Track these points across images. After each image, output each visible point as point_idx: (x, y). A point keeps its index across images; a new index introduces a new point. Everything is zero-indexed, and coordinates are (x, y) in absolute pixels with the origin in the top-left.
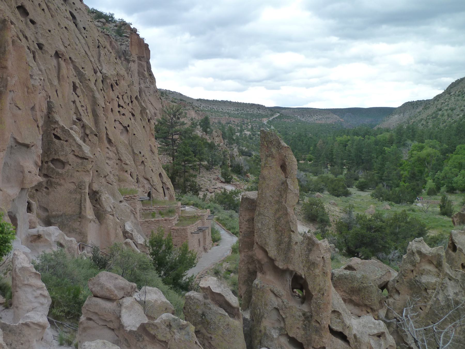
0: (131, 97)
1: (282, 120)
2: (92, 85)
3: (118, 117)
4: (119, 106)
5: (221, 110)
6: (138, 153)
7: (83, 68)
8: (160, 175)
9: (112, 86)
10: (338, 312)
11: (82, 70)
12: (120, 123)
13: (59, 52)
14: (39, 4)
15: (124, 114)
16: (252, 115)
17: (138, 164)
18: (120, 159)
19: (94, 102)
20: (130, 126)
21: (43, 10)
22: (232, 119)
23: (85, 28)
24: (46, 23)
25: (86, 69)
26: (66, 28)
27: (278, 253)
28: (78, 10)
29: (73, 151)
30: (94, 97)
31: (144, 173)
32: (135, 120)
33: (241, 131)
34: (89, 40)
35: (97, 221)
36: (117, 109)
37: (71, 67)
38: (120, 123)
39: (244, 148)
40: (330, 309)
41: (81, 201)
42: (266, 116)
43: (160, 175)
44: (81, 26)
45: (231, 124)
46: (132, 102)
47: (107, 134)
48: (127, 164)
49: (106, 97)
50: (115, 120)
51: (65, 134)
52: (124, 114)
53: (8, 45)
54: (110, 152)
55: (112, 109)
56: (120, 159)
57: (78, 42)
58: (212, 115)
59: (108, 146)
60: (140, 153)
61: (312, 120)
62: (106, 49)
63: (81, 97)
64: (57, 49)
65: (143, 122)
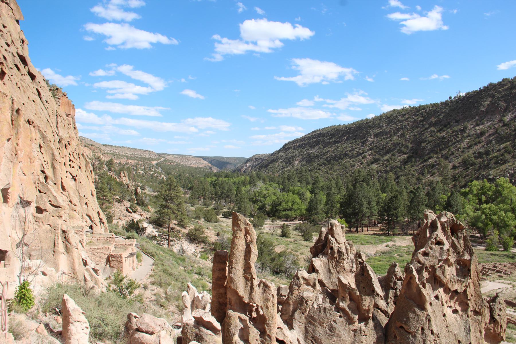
0: (79, 154)
1: (167, 163)
2: (52, 145)
3: (69, 169)
4: (70, 160)
5: (122, 154)
6: (83, 196)
7: (45, 132)
8: (98, 213)
9: (66, 146)
10: (281, 328)
11: (45, 133)
12: (71, 174)
13: (30, 121)
14: (17, 83)
15: (73, 167)
16: (145, 159)
17: (82, 204)
18: (71, 202)
19: (54, 159)
20: (78, 176)
21: (19, 88)
22: (130, 161)
23: (47, 102)
24: (21, 98)
25: (47, 133)
26: (34, 101)
27: (245, 293)
28: (42, 88)
29: (50, 201)
30: (53, 155)
31: (87, 211)
32: (81, 171)
33: (136, 170)
34: (50, 110)
35: (66, 253)
36: (68, 163)
37: (37, 131)
38: (71, 174)
39: (139, 183)
40: (277, 327)
41: (55, 238)
42: (155, 160)
43: (98, 213)
44: (44, 99)
45: (129, 164)
46: (79, 158)
47: (62, 183)
48: (75, 205)
49: (61, 154)
50: (67, 172)
51: (44, 188)
52: (73, 167)
53: (20, 128)
54: (63, 196)
55: (65, 163)
56: (71, 202)
57: (42, 112)
58: (114, 157)
59: (62, 191)
60: (85, 196)
61: (189, 164)
62: (62, 117)
63: (44, 154)
64: (29, 118)
65: (87, 173)
